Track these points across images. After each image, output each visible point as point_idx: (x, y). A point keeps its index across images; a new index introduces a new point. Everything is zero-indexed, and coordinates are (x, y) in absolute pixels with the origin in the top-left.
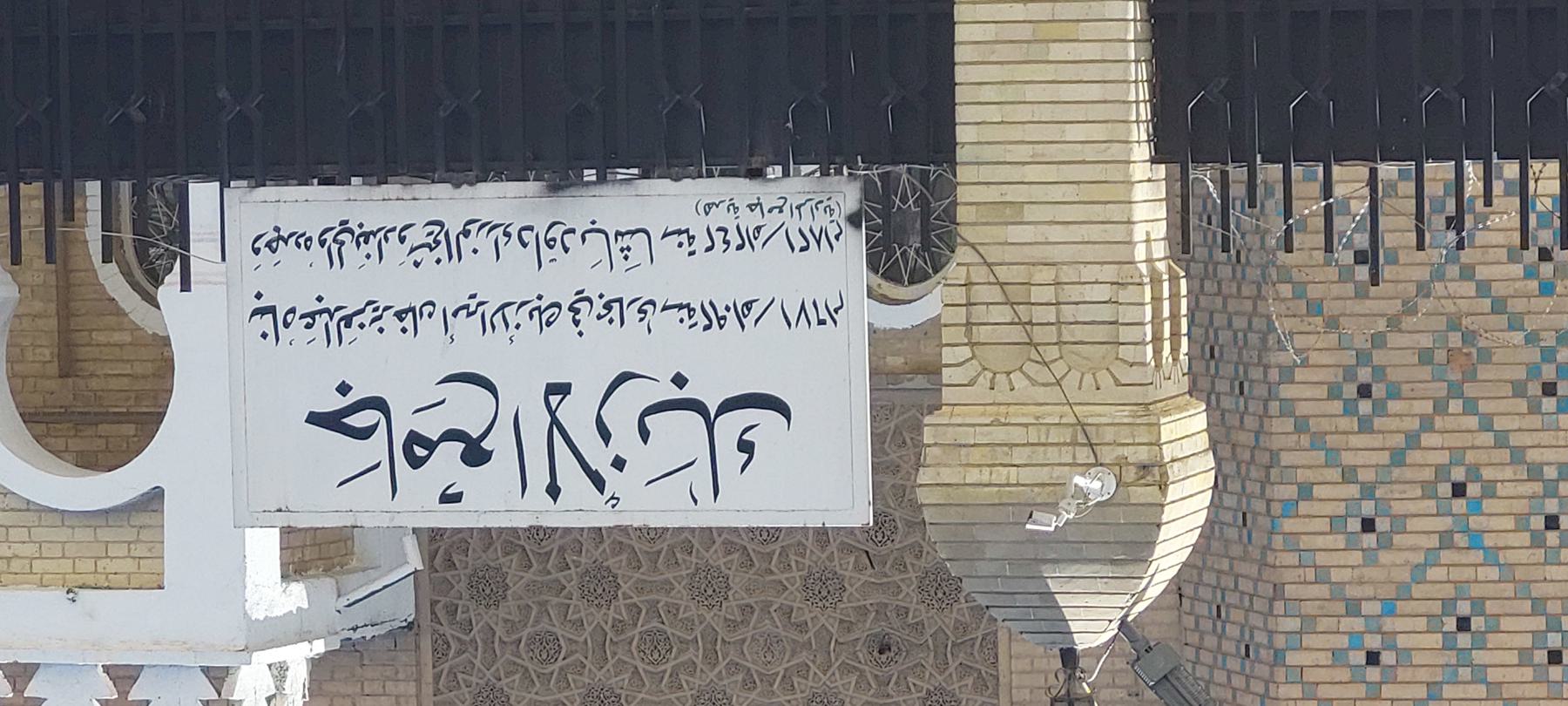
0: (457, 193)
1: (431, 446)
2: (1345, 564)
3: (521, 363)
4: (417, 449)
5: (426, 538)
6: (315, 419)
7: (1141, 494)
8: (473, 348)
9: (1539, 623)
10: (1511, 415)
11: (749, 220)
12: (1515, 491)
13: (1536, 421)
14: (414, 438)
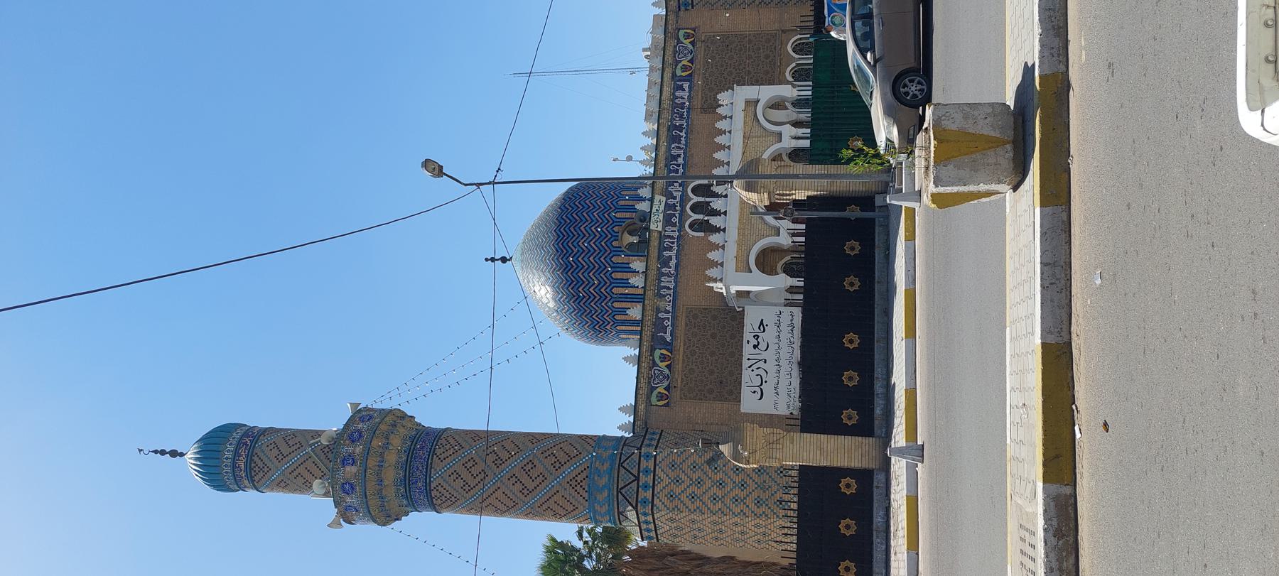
0: (797, 399)
3: (770, 355)
4: (756, 337)
5: (747, 211)
8: (772, 348)
10: (754, 495)
12: (742, 495)
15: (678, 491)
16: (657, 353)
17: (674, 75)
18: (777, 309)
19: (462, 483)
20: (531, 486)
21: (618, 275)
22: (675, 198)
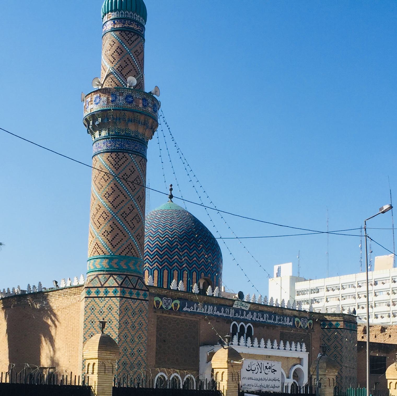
1: (269, 368)
2: (142, 347)
6: (276, 371)
7: (229, 361)
9: (127, 340)
11: (248, 387)
13: (126, 361)
14: (270, 369)
15: (98, 309)
16: (178, 302)
17: (295, 316)
18: (280, 379)
19: (129, 174)
20: (128, 219)
21: (176, 273)
22: (246, 316)
